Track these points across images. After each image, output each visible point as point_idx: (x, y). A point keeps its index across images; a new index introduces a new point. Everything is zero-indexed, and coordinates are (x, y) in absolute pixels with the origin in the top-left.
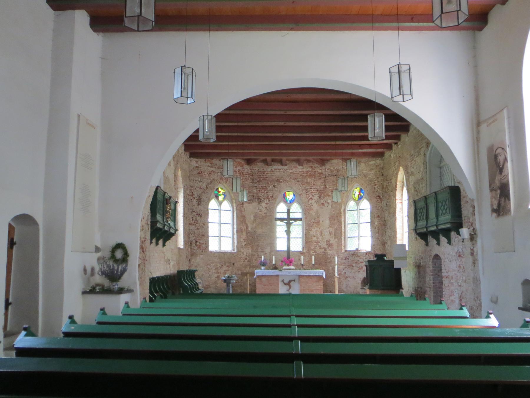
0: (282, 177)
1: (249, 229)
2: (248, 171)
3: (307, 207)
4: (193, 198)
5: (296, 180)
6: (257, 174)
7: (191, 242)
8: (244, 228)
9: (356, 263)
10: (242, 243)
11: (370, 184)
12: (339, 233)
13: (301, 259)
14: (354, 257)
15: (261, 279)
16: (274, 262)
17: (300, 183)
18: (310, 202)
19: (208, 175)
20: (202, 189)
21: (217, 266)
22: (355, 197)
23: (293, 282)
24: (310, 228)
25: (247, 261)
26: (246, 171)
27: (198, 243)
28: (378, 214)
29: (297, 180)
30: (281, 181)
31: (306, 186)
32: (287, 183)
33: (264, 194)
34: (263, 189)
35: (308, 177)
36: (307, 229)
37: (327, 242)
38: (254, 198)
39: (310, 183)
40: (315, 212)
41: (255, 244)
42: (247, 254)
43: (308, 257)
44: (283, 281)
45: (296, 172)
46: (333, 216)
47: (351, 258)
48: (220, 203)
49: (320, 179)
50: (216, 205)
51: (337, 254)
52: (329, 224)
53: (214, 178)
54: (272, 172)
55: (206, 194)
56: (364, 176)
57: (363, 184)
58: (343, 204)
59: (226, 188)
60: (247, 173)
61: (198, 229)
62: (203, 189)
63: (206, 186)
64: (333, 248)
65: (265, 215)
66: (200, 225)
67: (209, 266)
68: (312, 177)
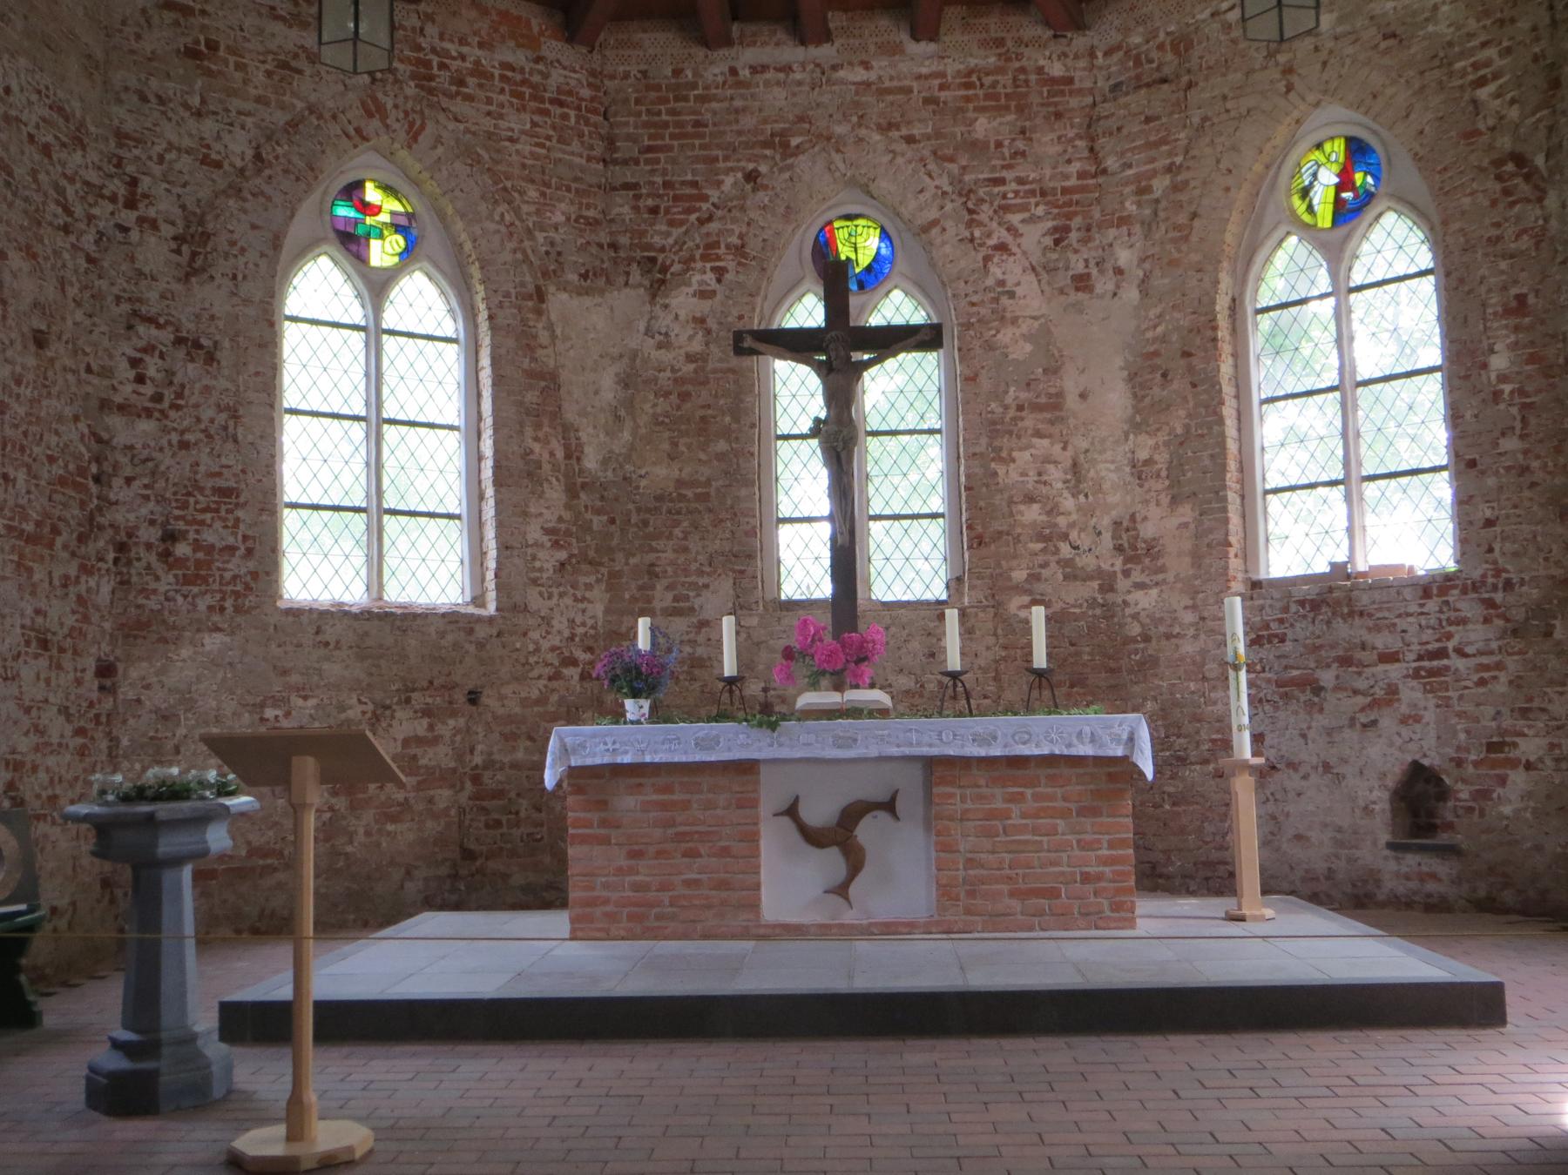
0: (801, 119)
1: (591, 462)
2: (573, 83)
3: (973, 304)
4: (141, 220)
5: (895, 134)
6: (638, 102)
7: (122, 537)
8: (552, 454)
9: (1345, 661)
10: (534, 558)
11: (1440, 82)
12: (1207, 462)
13: (944, 650)
14: (1328, 623)
15: (602, 805)
16: (729, 668)
17: (926, 153)
18: (996, 271)
19: (269, 74)
20: (218, 165)
21: (342, 708)
22: (1310, 209)
23: (882, 816)
24: (997, 443)
25: (572, 673)
26: (557, 77)
27: (182, 549)
28: (1514, 291)
29: (904, 132)
30: (795, 141)
31: (964, 168)
32: (838, 151)
33: (686, 233)
34: (676, 198)
35: (976, 109)
36: (978, 450)
37: (1114, 531)
38: (615, 262)
39: (992, 146)
40: (1027, 338)
41: (632, 561)
42: (580, 630)
43: (991, 640)
44: (792, 811)
45: (892, 78)
46: (1156, 354)
47: (1302, 630)
48: (376, 287)
49: (1058, 116)
50: (347, 291)
51: (1194, 607)
52: (1130, 411)
53: (313, 98)
54: (740, 84)
55: (247, 205)
56: (1385, 37)
57: (1375, 97)
58: (1225, 264)
59: (416, 183)
60: (570, 93)
61: (184, 445)
62: (226, 166)
63: (250, 153)
64: (1162, 569)
65: (692, 367)
66: (199, 420)
67: (279, 712)
68: (1007, 108)
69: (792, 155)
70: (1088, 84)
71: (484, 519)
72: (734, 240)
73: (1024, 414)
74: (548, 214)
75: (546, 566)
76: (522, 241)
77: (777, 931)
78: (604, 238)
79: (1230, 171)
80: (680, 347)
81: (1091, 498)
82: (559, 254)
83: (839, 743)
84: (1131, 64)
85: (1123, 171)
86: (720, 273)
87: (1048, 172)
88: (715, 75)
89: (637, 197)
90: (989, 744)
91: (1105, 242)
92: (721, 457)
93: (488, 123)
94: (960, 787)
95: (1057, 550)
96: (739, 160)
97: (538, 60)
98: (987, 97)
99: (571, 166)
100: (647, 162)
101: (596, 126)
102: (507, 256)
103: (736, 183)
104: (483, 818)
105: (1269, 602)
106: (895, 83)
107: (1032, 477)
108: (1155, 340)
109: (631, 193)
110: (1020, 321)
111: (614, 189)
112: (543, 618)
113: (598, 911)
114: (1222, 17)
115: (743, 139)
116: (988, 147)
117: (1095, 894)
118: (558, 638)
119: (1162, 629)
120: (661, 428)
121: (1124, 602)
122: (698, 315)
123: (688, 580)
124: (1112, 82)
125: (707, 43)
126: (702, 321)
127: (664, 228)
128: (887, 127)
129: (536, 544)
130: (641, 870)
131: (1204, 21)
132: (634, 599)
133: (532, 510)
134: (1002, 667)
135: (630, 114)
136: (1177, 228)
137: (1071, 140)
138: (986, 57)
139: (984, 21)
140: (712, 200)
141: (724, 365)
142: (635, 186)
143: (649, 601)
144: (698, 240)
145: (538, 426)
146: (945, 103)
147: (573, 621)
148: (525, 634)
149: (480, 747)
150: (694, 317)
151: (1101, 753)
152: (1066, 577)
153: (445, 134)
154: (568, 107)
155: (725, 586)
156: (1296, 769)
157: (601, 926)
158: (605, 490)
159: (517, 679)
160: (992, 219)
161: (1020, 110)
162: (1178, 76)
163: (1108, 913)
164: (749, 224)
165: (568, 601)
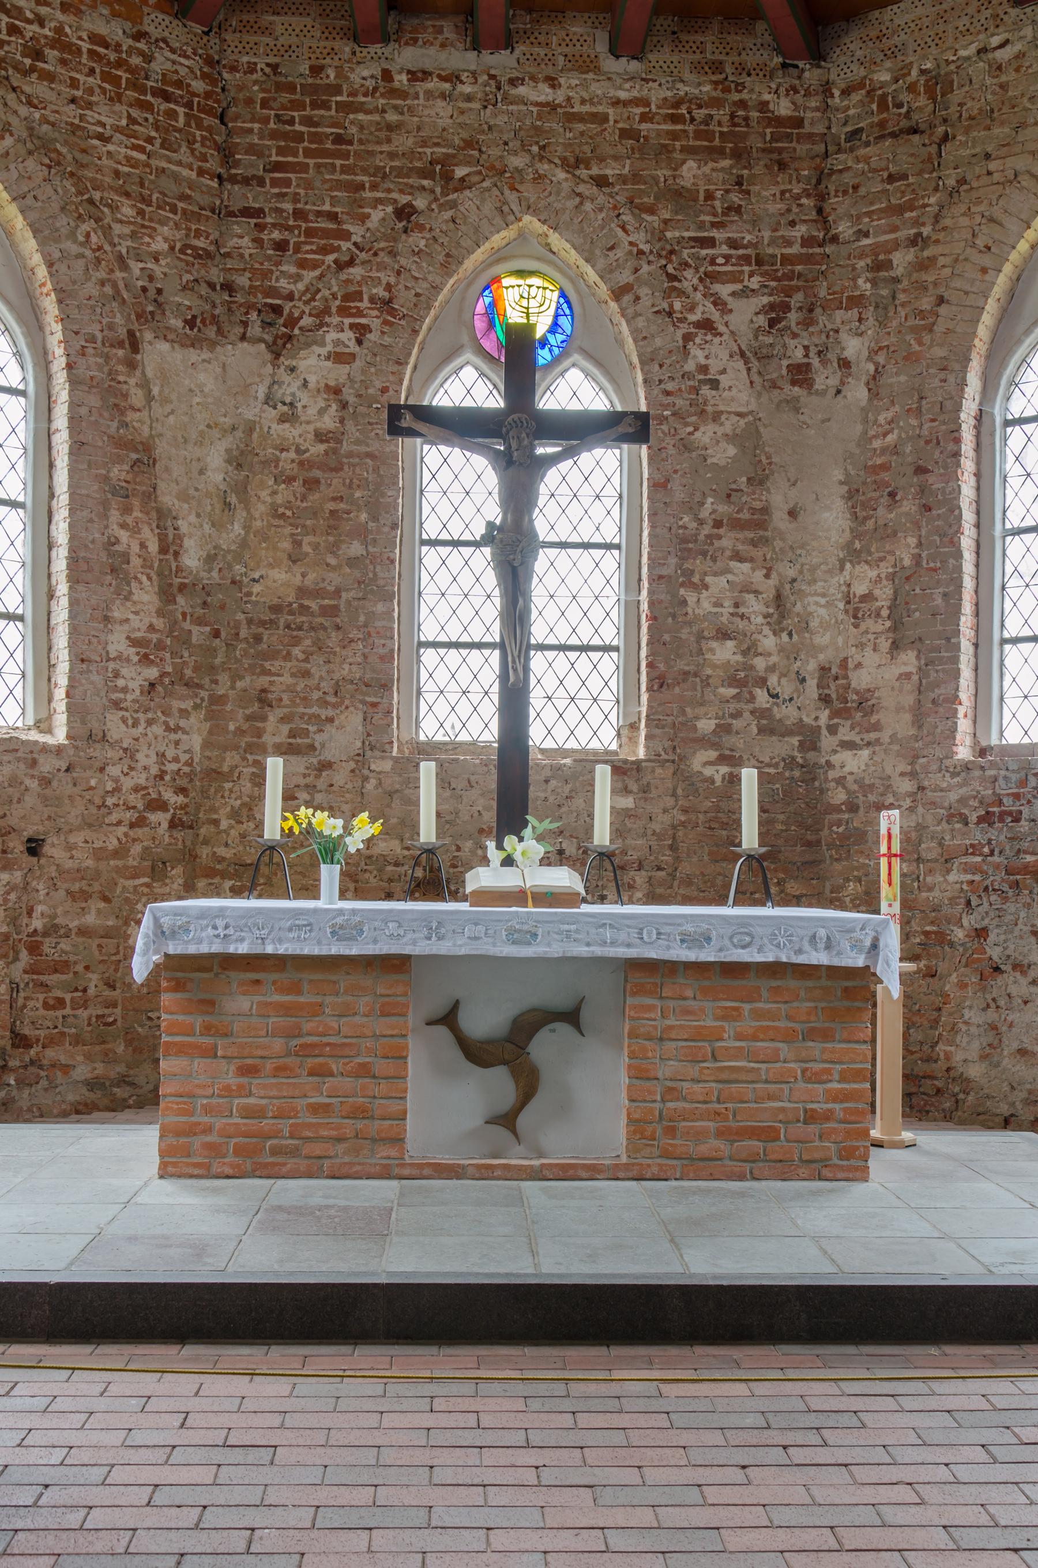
1: (192, 559)
2: (183, 72)
3: (668, 393)
5: (583, 173)
8: (143, 545)
10: (117, 675)
12: (939, 601)
15: (208, 1005)
18: (698, 354)
23: (563, 1029)
25: (161, 818)
26: (161, 63)
29: (595, 171)
30: (460, 172)
31: (666, 222)
32: (513, 188)
34: (310, 233)
36: (664, 571)
37: (821, 678)
41: (239, 684)
42: (174, 767)
43: (670, 801)
44: (449, 1019)
45: (583, 102)
46: (885, 467)
49: (782, 166)
51: (913, 775)
52: (847, 535)
64: (876, 727)
65: (322, 448)
68: (721, 152)
69: (456, 190)
70: (820, 129)
71: (53, 622)
72: (380, 292)
73: (722, 531)
74: (147, 239)
75: (132, 685)
76: (112, 271)
77: (426, 1172)
78: (215, 275)
79: (989, 249)
80: (308, 423)
81: (795, 637)
82: (159, 291)
83: (515, 936)
84: (874, 107)
85: (858, 240)
86: (361, 332)
87: (767, 234)
88: (364, 78)
89: (260, 227)
90: (702, 947)
91: (829, 326)
92: (353, 562)
93: (71, 112)
94: (661, 998)
95: (752, 698)
96: (389, 191)
97: (139, 36)
98: (698, 135)
99: (176, 178)
100: (275, 183)
101: (210, 129)
102: (91, 288)
103: (384, 219)
104: (41, 997)
105: (1003, 773)
106: (586, 108)
107: (728, 608)
108: (884, 450)
109: (253, 221)
110: (723, 417)
111: (231, 214)
112: (125, 750)
113: (197, 1142)
114: (990, 56)
115: (396, 163)
116: (696, 200)
117: (820, 1137)
118: (144, 776)
119: (872, 798)
120: (282, 523)
121: (828, 762)
122: (332, 383)
123: (307, 711)
124: (849, 128)
125: (358, 37)
126: (337, 391)
127: (293, 270)
128: (573, 164)
129: (119, 657)
130: (254, 1090)
131: (968, 58)
132: (240, 732)
133: (116, 614)
134: (680, 833)
135: (253, 120)
136: (921, 314)
137: (798, 197)
138: (699, 84)
139: (699, 38)
140: (354, 238)
141: (363, 449)
142: (259, 213)
143: (259, 733)
144: (335, 289)
145: (127, 510)
146: (646, 138)
147: (163, 755)
148: (102, 770)
149: (39, 909)
150: (327, 385)
151: (836, 962)
152: (761, 731)
153: (15, 121)
154: (176, 103)
155: (353, 721)
156: (1024, 973)
157: (199, 1160)
158: (208, 594)
159: (90, 826)
160: (695, 289)
161: (737, 155)
162: (932, 126)
163: (836, 1161)
164: (399, 273)
165: (157, 729)
